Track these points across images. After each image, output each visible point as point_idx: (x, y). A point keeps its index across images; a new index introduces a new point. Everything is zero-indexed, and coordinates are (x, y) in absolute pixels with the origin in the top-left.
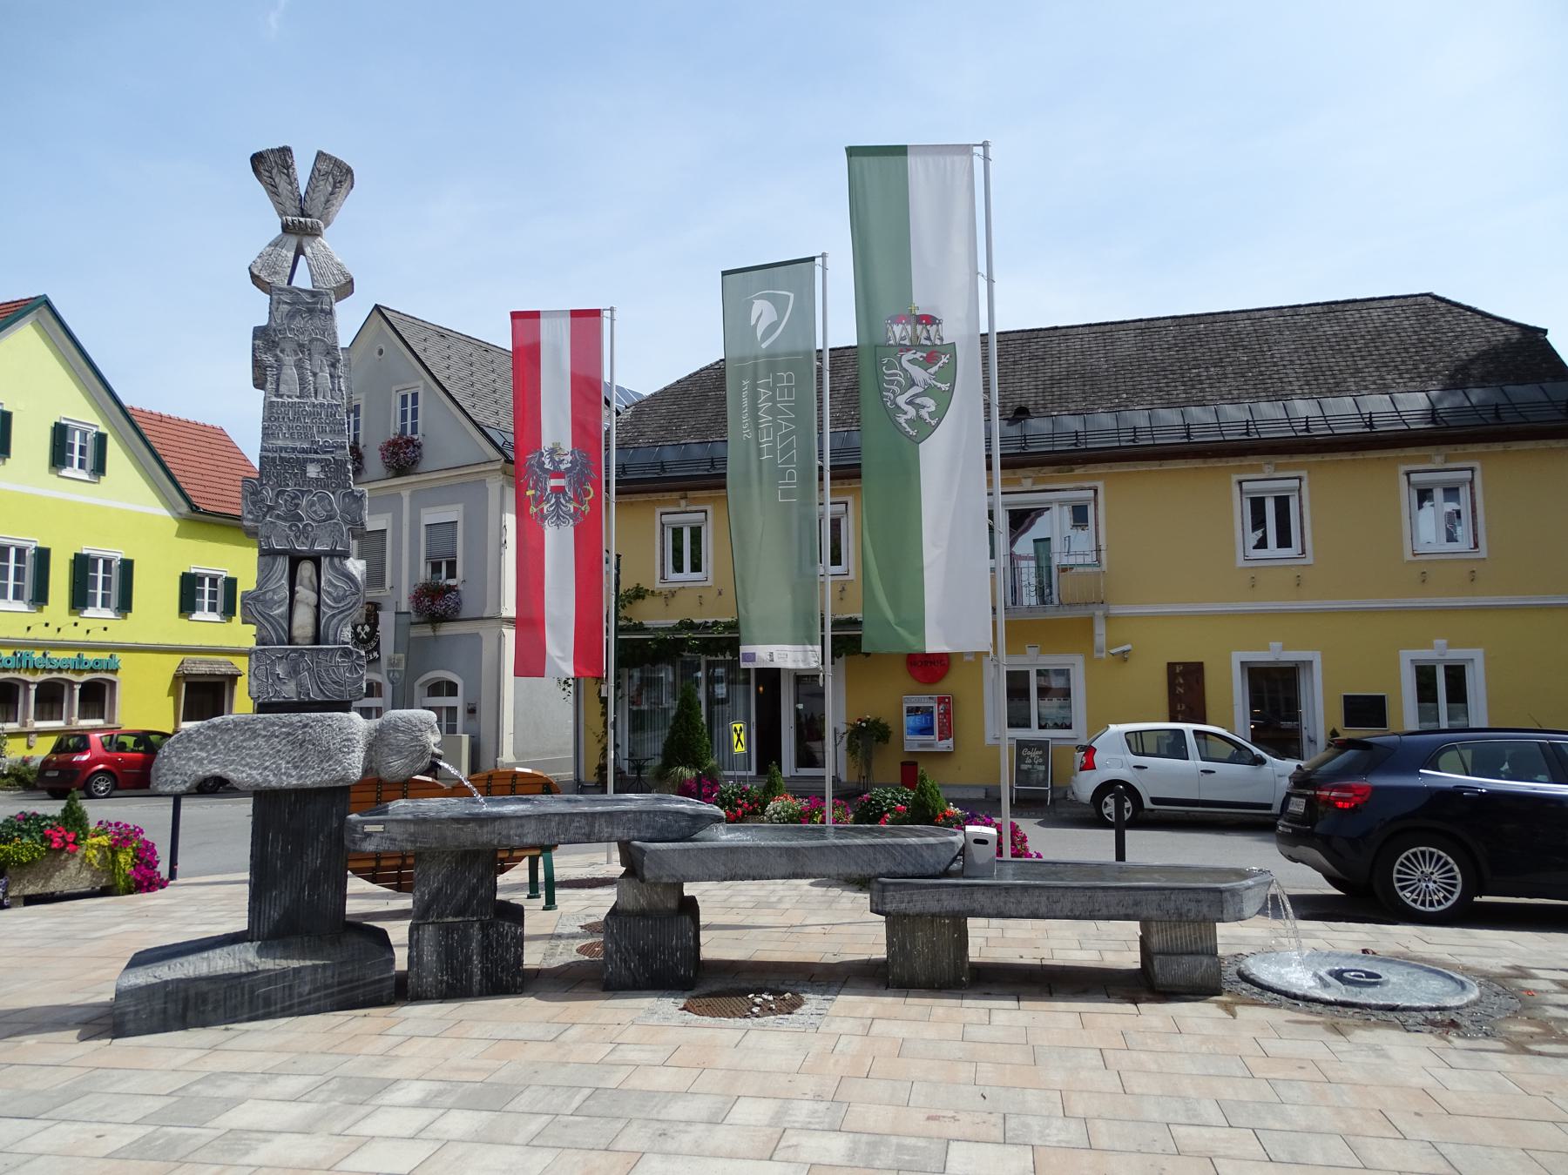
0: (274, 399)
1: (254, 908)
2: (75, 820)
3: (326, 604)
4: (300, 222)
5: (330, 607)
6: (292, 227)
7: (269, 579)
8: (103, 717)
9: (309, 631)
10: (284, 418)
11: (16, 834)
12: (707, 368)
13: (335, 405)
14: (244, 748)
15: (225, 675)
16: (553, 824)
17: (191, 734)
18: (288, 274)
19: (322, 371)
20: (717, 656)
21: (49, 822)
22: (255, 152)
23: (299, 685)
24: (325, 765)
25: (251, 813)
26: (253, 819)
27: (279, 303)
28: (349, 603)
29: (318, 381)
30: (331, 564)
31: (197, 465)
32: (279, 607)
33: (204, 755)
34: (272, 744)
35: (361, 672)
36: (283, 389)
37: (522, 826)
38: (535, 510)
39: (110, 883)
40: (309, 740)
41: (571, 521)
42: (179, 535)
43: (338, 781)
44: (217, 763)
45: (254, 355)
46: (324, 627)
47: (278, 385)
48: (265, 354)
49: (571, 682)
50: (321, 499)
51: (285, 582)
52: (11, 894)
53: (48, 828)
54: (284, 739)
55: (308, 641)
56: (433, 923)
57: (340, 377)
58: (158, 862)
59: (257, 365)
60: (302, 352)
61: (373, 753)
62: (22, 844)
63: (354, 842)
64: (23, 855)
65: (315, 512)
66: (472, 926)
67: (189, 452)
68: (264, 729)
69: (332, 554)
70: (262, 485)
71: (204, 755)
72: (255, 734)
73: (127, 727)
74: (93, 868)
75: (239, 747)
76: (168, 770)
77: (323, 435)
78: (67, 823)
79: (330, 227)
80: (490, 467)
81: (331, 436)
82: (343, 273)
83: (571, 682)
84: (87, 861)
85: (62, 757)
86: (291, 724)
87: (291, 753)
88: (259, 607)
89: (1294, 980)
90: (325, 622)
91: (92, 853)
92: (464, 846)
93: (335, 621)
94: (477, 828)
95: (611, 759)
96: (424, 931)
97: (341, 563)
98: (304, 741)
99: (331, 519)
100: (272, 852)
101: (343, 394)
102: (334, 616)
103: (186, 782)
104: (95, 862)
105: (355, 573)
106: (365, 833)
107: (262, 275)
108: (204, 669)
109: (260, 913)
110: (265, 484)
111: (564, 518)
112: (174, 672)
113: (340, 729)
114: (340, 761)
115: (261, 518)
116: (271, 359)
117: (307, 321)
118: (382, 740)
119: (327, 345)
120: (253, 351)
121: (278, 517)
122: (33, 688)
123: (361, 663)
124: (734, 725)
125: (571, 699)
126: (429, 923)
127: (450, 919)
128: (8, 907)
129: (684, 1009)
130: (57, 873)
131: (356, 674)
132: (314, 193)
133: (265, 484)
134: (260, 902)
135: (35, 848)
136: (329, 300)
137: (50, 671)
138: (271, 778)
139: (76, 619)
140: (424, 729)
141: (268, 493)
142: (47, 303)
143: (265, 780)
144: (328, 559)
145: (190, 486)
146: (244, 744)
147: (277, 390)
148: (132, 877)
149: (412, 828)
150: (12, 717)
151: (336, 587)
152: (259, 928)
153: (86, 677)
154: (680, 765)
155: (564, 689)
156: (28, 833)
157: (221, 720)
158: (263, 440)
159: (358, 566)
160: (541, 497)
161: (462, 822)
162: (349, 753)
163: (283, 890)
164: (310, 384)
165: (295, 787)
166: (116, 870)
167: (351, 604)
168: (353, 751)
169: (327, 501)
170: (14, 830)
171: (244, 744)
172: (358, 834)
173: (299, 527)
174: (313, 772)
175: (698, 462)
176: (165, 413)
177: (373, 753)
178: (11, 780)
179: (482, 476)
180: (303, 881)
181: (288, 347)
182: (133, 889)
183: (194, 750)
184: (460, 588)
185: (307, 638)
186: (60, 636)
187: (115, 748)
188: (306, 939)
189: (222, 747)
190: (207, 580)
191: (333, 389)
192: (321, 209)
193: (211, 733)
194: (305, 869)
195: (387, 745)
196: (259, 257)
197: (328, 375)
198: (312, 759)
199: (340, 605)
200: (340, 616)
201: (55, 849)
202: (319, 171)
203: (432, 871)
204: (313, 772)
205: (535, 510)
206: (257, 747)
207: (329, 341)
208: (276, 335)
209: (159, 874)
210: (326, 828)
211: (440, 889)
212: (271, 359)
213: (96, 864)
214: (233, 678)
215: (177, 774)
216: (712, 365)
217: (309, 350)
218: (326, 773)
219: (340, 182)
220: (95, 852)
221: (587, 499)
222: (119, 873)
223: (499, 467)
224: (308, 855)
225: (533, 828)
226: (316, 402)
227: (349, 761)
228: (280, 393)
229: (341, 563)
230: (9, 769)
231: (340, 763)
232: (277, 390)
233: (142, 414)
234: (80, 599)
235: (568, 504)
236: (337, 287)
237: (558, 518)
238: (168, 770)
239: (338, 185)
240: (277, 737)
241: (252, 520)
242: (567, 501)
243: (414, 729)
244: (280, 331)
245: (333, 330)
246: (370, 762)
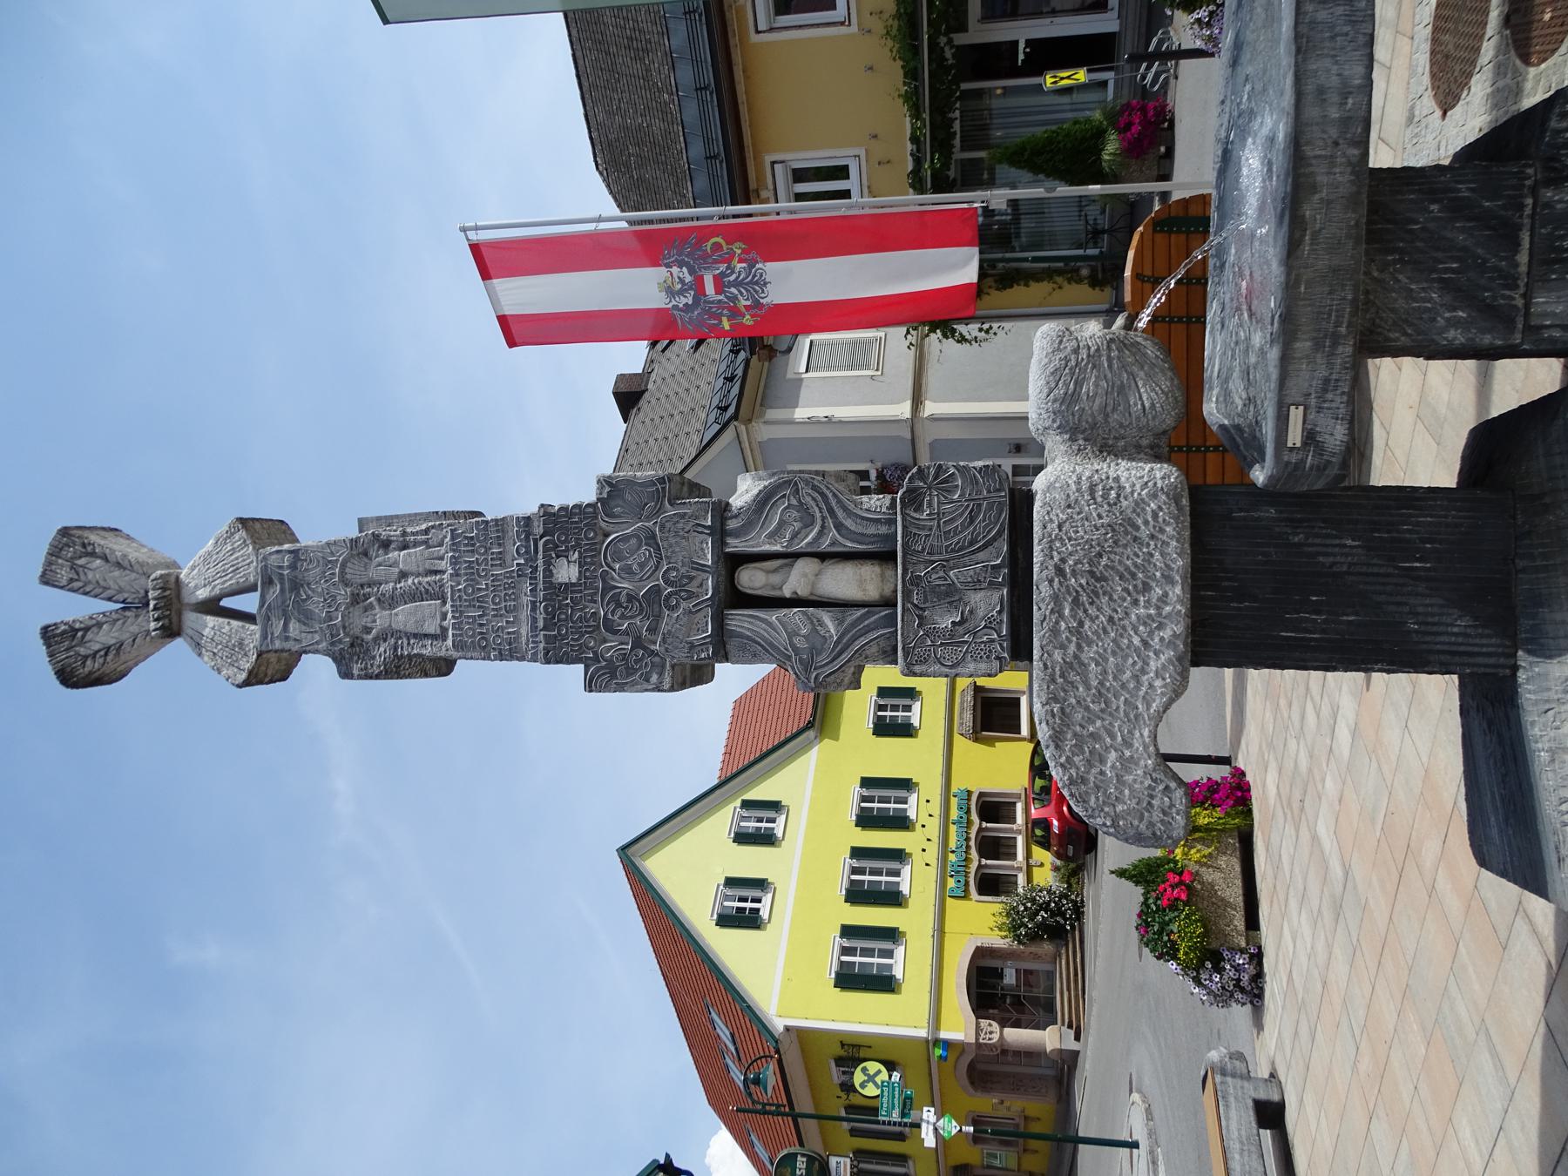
0: (449, 642)
1: (1442, 664)
2: (1150, 872)
3: (816, 540)
4: (155, 609)
5: (821, 533)
6: (167, 621)
7: (771, 645)
8: (1015, 803)
9: (870, 571)
10: (481, 625)
11: (1166, 938)
12: (608, 186)
13: (453, 538)
14: (1101, 683)
15: (975, 697)
16: (1322, 15)
17: (1070, 778)
18: (240, 624)
19: (395, 564)
20: (955, 133)
21: (1151, 901)
22: (57, 683)
23: (976, 585)
24: (1144, 532)
25: (1360, 676)
26: (1258, 664)
27: (287, 639)
28: (814, 499)
29: (414, 568)
30: (737, 533)
31: (769, 722)
32: (821, 623)
33: (1113, 755)
34: (1096, 633)
35: (952, 470)
36: (431, 627)
37: (1321, 91)
38: (748, 317)
39: (1236, 834)
40: (1091, 563)
41: (757, 266)
42: (836, 739)
43: (1180, 508)
44: (1130, 732)
45: (378, 677)
46: (860, 543)
47: (426, 636)
48: (374, 658)
49: (986, 326)
50: (618, 557)
51: (774, 616)
52: (1243, 944)
53: (1159, 902)
54: (1085, 611)
55: (889, 573)
56: (1527, 297)
57: (404, 534)
58: (1209, 779)
59: (397, 669)
60: (367, 596)
61: (1121, 443)
62: (1179, 932)
63: (1321, 469)
64: (1194, 932)
65: (642, 565)
66: (1549, 205)
67: (757, 730)
68: (1063, 647)
69: (720, 533)
70: (596, 659)
71: (1113, 755)
72: (1075, 664)
73: (1026, 783)
74: (1215, 853)
75: (1099, 692)
76: (1141, 819)
77: (508, 559)
78: (1154, 882)
79: (178, 562)
80: (744, 437)
81: (509, 543)
82: (230, 534)
83: (986, 326)
84: (1205, 860)
85: (1054, 841)
86: (1056, 598)
87: (1115, 597)
88: (822, 659)
90: (852, 541)
91: (1194, 854)
92: (1357, 224)
93: (849, 523)
94: (1317, 196)
95: (1101, 189)
96: (1545, 315)
97: (736, 516)
98: (1091, 573)
99: (654, 536)
100: (1323, 631)
101: (433, 527)
102: (839, 526)
103: (1167, 787)
104: (1207, 851)
105: (755, 491)
106: (1304, 444)
107: (248, 666)
108: (968, 716)
109: (1453, 653)
110: (595, 653)
111: (755, 276)
112: (970, 742)
113: (1069, 506)
114: (1137, 504)
115: (657, 659)
116: (382, 649)
117: (313, 591)
118: (1094, 426)
119: (352, 556)
120: (371, 678)
121: (653, 630)
123: (932, 471)
124: (1048, 85)
125: (1007, 325)
126: (1527, 306)
127: (1523, 258)
128: (1260, 948)
129: (1445, 114)
130: (1219, 893)
131: (956, 480)
132: (109, 589)
133: (595, 653)
134: (1430, 652)
135: (1185, 918)
136: (273, 557)
137: (968, 847)
138: (1167, 634)
139: (918, 826)
140: (1074, 343)
141: (611, 647)
142: (624, 850)
143: (1171, 644)
144: (729, 540)
145: (789, 729)
146: (1094, 683)
147: (434, 637)
148: (1229, 810)
149: (1303, 346)
150: (1013, 879)
151: (782, 524)
152: (1489, 655)
153: (975, 817)
154: (1099, 159)
155: (995, 334)
156: (1164, 925)
157: (1044, 725)
158: (522, 659)
159: (745, 487)
160: (730, 308)
161: (1297, 234)
162: (1121, 488)
163: (1407, 609)
164: (420, 583)
165: (1188, 589)
166: (1219, 827)
167: (816, 495)
168: (1117, 479)
169: (621, 546)
170: (1160, 938)
171: (1094, 683)
172: (1303, 461)
173: (670, 594)
174: (1157, 555)
175: (712, 177)
176: (723, 751)
177: (1121, 443)
178: (1073, 881)
179: (755, 446)
180: (1390, 570)
181: (358, 620)
182: (1245, 809)
183: (1102, 773)
184: (879, 465)
185: (882, 575)
186: (935, 839)
187: (1047, 797)
188: (1521, 564)
189: (1099, 723)
190: (880, 713)
191: (426, 542)
192: (134, 575)
193: (1069, 744)
194: (1364, 569)
195: (1107, 416)
196: (219, 671)
197: (402, 553)
198: (1130, 557)
199: (818, 515)
200: (840, 514)
201: (1188, 895)
202: (71, 580)
203: (1401, 304)
204: (1157, 555)
205: (748, 317)
206: (1101, 660)
207: (343, 553)
208: (340, 641)
209: (1224, 778)
210: (1277, 529)
211: (1446, 285)
212: (382, 649)
213: (1210, 850)
214: (978, 689)
215: (1149, 803)
216: (604, 180)
217: (362, 586)
218: (1162, 531)
219: (84, 546)
220: (1193, 851)
221: (725, 247)
222: (1223, 824)
223: (743, 427)
224: (1333, 564)
225: (1327, 62)
226: (450, 571)
227: (1138, 487)
228: (438, 632)
229: (736, 516)
230: (1063, 883)
231: (1139, 504)
232: (434, 637)
233: (724, 770)
234: (901, 822)
235: (737, 270)
236: (254, 543)
237: (757, 283)
238: (1141, 819)
239: (89, 549)
240: (1081, 624)
241: (661, 674)
242: (733, 272)
243: (1073, 363)
244: (332, 636)
245: (322, 547)
246: (1139, 448)
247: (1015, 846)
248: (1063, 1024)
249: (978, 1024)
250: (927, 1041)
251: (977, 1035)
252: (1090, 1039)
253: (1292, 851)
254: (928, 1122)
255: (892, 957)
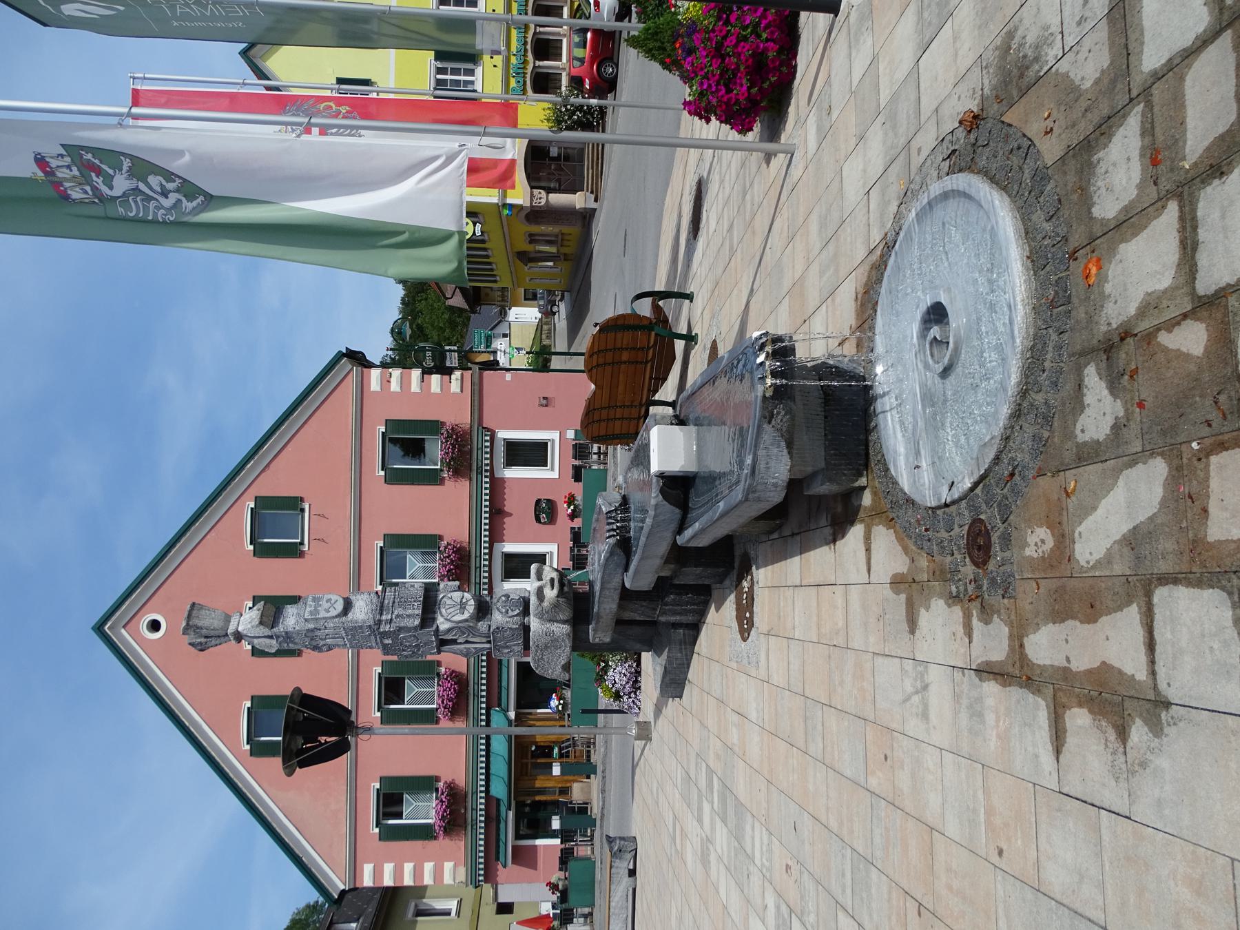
89: (1009, 411)
122: (538, 63)
137: (526, 51)
150: (559, 77)
247: (561, 48)
248: (587, 191)
249: (532, 193)
250: (498, 204)
251: (531, 200)
252: (605, 202)
253: (747, 162)
254: (501, 351)
255: (473, 75)
